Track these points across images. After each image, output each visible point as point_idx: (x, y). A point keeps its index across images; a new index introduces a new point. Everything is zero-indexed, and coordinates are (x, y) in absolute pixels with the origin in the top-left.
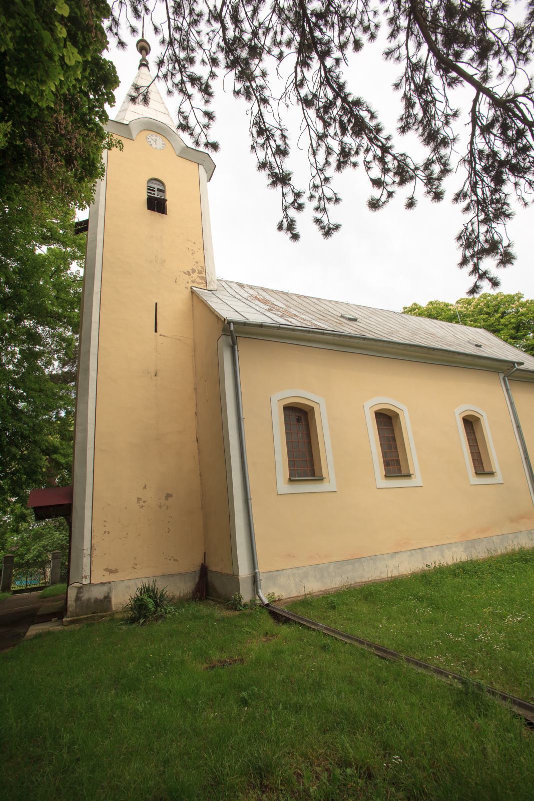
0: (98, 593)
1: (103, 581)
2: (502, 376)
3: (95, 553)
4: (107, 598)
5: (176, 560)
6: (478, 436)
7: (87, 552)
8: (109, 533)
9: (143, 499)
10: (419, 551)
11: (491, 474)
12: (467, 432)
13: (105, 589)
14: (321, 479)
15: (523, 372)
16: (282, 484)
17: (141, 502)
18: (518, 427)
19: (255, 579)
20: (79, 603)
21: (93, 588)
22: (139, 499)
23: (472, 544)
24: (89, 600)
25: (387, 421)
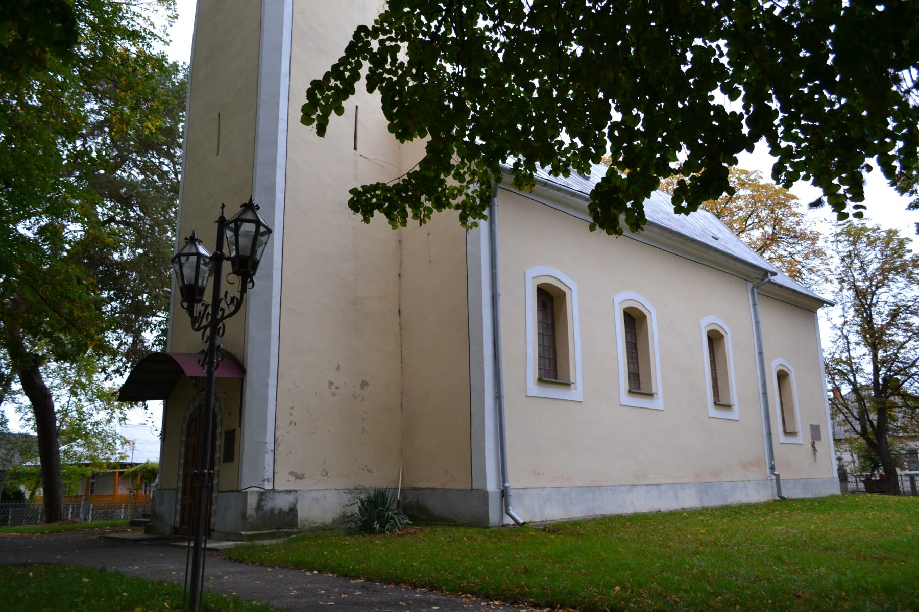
0: (282, 503)
1: (289, 488)
2: (750, 285)
3: (280, 449)
4: (293, 510)
5: (369, 471)
6: (718, 358)
7: (270, 447)
8: (295, 424)
9: (336, 384)
10: (655, 487)
11: (728, 407)
12: (626, 332)
13: (290, 498)
15: (738, 264)
16: (533, 388)
17: (333, 387)
18: (761, 353)
20: (260, 513)
21: (277, 496)
22: (331, 383)
23: (704, 488)
24: (272, 510)
25: (634, 320)
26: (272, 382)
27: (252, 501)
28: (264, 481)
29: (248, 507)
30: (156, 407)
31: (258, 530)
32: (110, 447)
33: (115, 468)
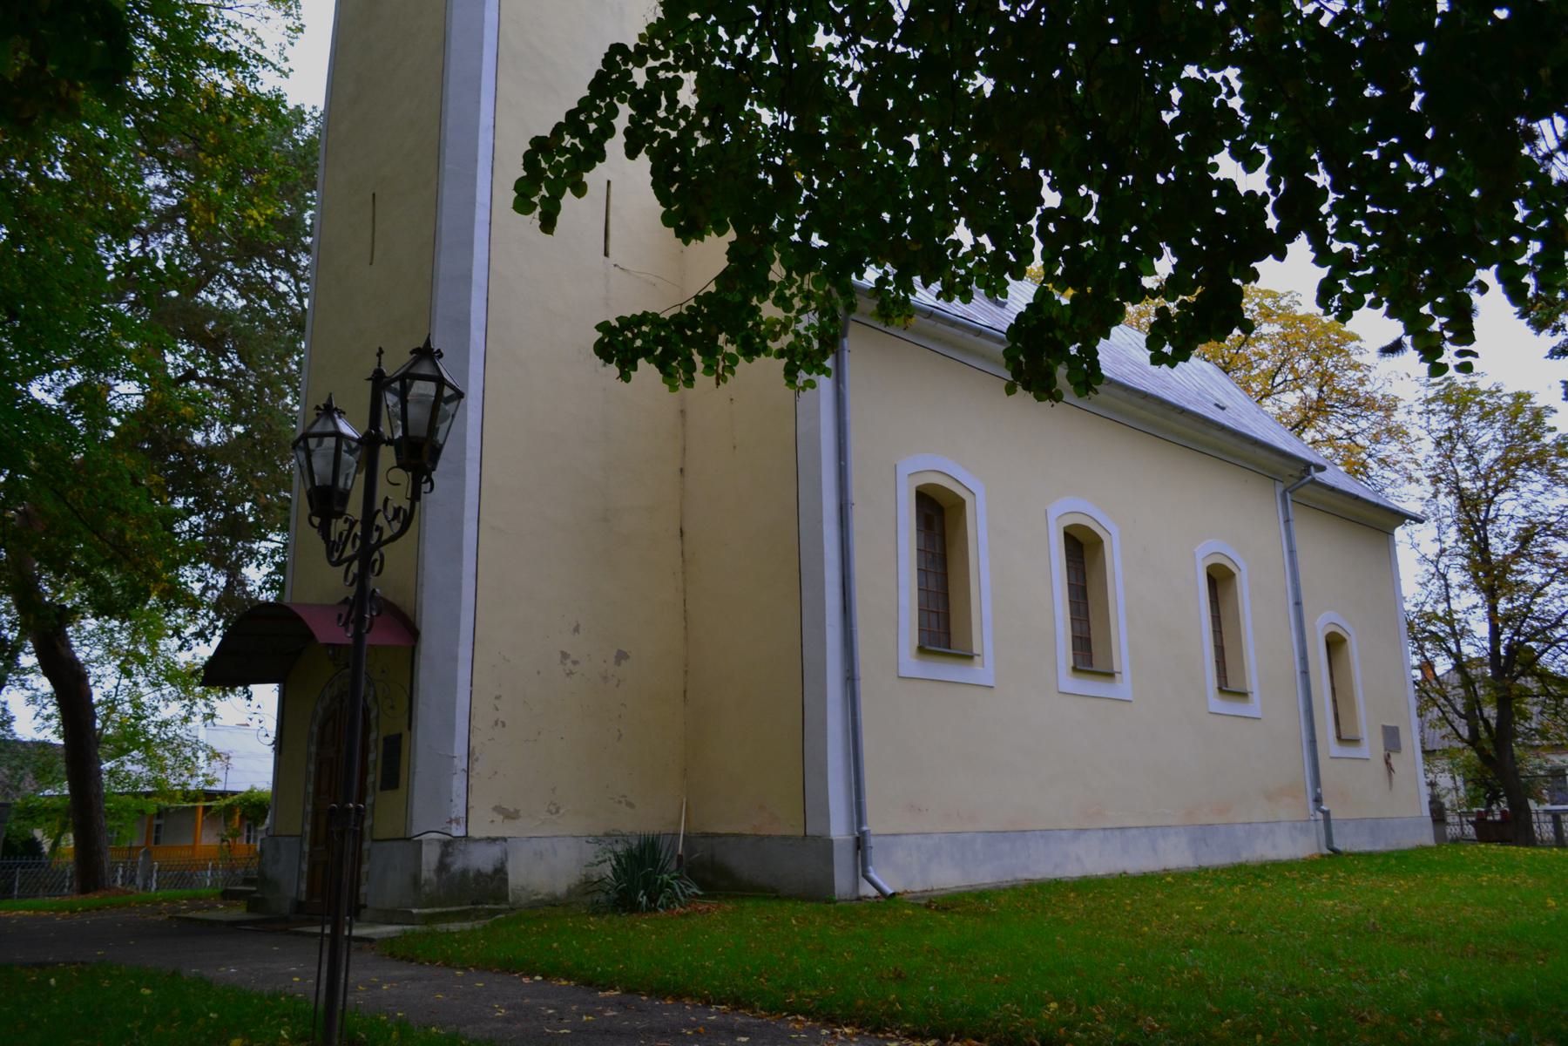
0: (481, 859)
1: (493, 835)
2: (1280, 488)
3: (476, 768)
4: (500, 872)
5: (630, 805)
7: (461, 764)
10: (1117, 833)
11: (1243, 695)
13: (495, 851)
14: (968, 657)
16: (909, 662)
17: (569, 662)
18: (1298, 604)
19: (860, 844)
20: (444, 876)
21: (472, 846)
22: (565, 655)
23: (1200, 834)
24: (465, 872)
25: (1082, 548)
26: (464, 652)
27: (430, 856)
28: (450, 822)
29: (424, 867)
30: (267, 695)
31: (440, 905)
32: (188, 764)
33: (196, 800)
